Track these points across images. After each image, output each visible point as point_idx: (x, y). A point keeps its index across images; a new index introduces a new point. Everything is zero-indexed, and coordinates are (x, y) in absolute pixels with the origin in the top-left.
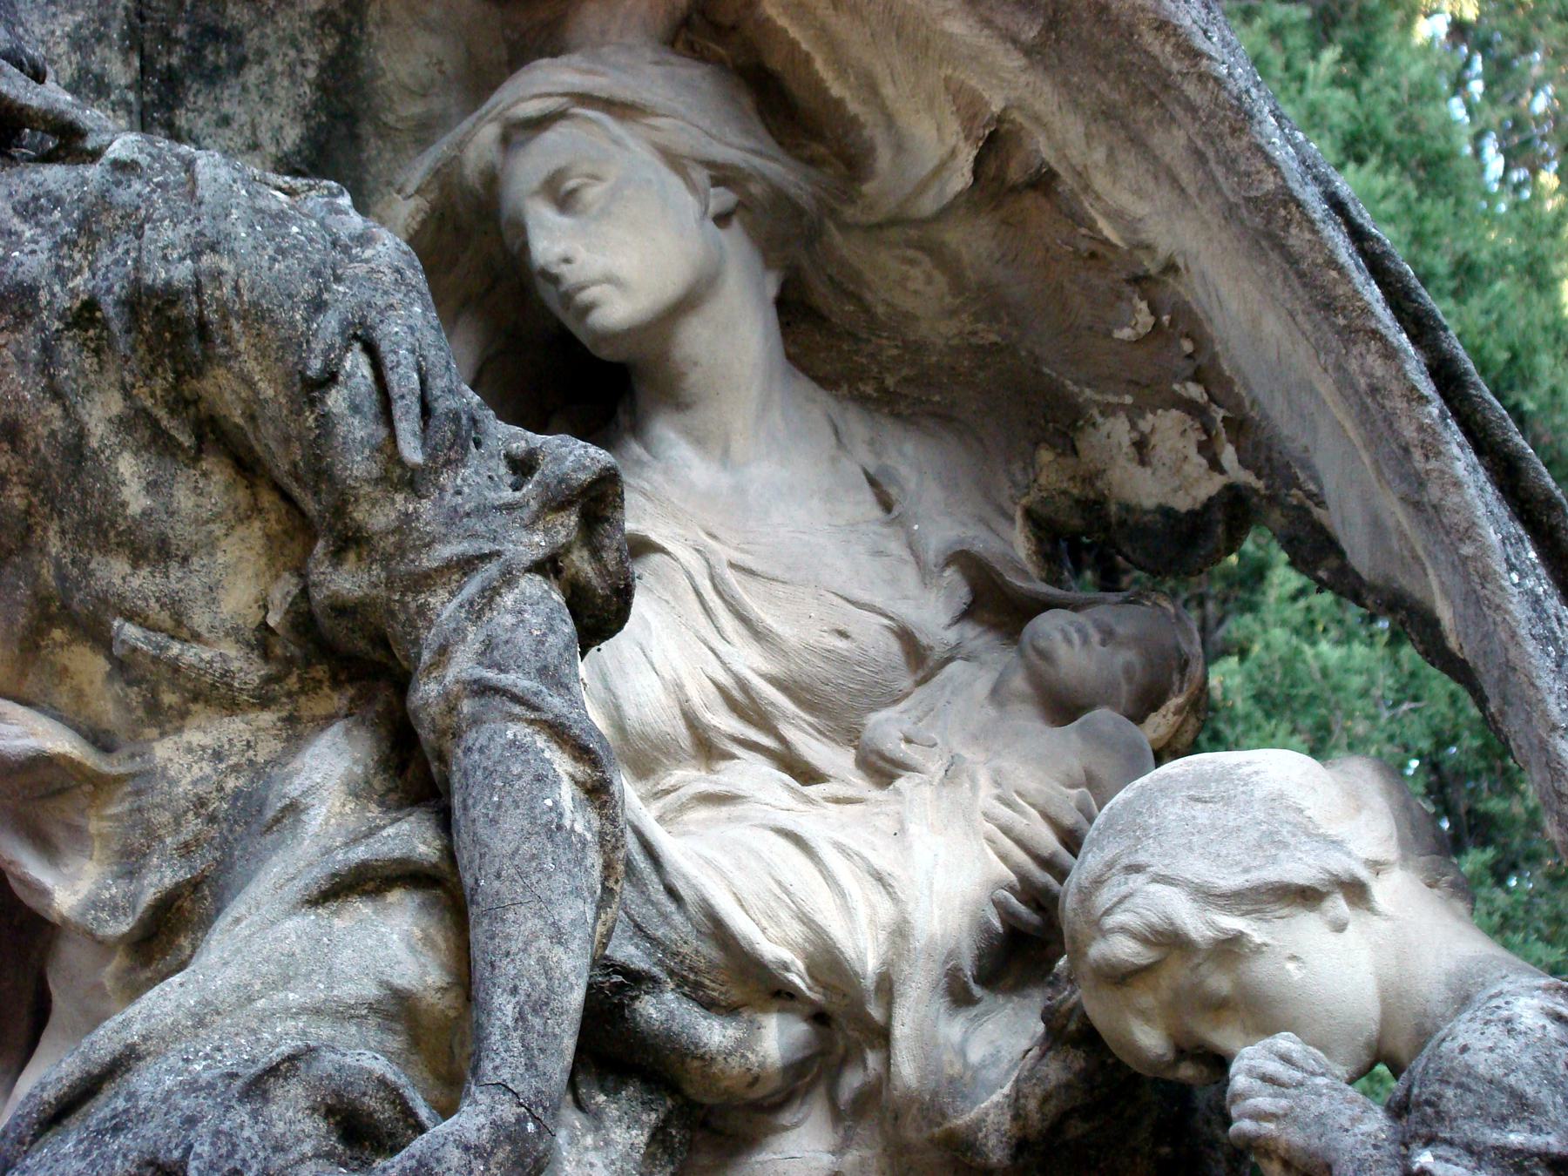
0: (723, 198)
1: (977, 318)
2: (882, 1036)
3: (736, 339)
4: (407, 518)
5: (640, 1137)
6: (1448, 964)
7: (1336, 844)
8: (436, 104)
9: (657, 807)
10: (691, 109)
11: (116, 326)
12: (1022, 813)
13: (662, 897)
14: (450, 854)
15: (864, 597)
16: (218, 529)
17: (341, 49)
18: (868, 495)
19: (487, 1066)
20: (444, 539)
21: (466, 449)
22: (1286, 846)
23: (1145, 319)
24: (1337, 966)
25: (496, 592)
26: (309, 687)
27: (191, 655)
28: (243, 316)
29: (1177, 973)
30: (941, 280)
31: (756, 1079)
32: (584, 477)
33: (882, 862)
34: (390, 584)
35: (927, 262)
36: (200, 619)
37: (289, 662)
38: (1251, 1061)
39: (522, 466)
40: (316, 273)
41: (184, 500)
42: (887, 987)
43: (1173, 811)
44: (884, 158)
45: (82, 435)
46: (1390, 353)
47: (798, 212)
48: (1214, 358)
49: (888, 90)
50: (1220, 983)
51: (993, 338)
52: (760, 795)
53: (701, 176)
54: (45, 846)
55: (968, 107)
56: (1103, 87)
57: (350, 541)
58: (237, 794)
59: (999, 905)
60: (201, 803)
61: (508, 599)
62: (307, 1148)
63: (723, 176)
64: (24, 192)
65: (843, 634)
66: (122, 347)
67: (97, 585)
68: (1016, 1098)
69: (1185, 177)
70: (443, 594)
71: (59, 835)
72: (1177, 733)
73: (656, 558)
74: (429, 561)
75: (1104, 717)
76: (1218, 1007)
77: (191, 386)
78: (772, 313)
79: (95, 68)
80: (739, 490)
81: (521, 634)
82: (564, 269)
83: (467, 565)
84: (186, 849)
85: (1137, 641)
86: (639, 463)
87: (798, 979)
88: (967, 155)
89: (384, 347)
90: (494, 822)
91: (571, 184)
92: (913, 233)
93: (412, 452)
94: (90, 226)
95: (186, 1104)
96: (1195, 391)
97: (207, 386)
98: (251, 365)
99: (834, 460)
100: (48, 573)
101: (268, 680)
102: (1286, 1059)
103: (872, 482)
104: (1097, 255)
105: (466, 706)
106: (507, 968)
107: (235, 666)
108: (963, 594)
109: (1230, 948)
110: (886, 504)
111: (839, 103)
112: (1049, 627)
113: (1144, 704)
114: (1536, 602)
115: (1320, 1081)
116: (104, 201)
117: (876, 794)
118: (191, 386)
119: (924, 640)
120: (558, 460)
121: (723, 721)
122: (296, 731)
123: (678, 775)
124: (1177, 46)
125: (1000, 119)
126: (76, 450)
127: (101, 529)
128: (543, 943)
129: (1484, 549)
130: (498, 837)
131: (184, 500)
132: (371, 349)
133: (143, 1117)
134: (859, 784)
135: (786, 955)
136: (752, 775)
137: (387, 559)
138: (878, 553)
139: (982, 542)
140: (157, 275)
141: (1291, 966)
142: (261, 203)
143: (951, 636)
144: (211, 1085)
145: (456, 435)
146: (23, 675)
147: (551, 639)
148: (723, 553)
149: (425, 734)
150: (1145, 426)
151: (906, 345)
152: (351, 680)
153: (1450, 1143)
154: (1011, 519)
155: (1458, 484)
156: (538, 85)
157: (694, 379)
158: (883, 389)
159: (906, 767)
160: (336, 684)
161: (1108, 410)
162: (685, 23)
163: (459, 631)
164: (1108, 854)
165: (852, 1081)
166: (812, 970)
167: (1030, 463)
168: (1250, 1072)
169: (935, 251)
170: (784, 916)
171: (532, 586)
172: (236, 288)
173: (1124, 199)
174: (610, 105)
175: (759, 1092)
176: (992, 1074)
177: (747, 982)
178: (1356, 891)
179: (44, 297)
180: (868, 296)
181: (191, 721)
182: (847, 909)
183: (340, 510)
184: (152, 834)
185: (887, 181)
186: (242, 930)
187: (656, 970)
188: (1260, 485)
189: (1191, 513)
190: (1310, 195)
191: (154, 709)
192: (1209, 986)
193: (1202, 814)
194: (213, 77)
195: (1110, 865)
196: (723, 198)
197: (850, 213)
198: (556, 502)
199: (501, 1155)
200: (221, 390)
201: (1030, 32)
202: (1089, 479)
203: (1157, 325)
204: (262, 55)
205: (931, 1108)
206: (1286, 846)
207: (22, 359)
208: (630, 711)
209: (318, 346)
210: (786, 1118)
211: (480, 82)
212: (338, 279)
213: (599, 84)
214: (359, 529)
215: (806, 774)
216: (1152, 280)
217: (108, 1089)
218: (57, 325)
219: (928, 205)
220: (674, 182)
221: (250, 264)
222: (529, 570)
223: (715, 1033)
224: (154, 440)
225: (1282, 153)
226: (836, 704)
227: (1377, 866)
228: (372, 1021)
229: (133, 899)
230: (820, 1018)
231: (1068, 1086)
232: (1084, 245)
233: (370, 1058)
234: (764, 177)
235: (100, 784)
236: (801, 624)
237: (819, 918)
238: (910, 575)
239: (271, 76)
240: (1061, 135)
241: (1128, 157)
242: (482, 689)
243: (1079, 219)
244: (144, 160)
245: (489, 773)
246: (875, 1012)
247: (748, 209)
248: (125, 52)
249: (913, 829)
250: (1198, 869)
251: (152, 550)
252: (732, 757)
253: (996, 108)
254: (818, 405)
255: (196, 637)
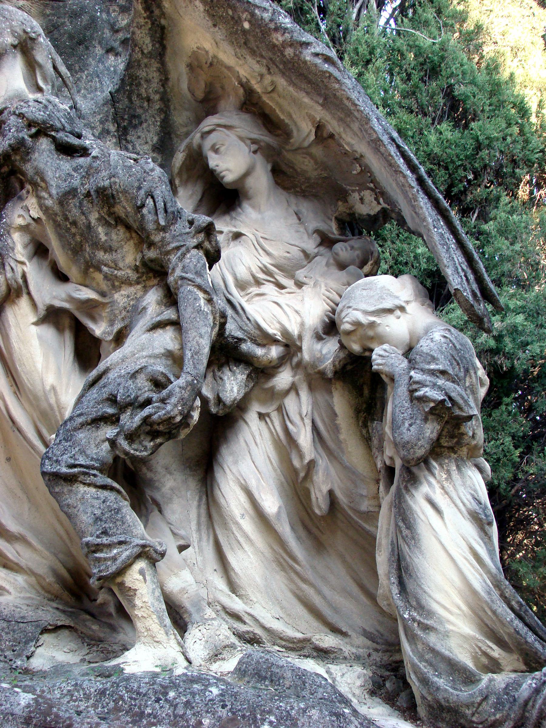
0: (254, 147)
1: (322, 170)
2: (300, 349)
3: (261, 181)
4: (163, 238)
5: (244, 377)
6: (424, 325)
7: (397, 297)
8: (190, 128)
9: (246, 298)
10: (245, 126)
11: (94, 197)
12: (332, 293)
13: (246, 320)
14: (179, 317)
15: (293, 243)
16: (123, 243)
17: (165, 117)
18: (295, 217)
19: (185, 368)
20: (172, 243)
21: (177, 220)
22: (384, 299)
23: (359, 169)
24: (397, 327)
25: (185, 254)
26: (149, 279)
27: (119, 273)
28: (122, 192)
29: (360, 332)
30: (312, 162)
31: (271, 362)
32: (204, 225)
33: (297, 308)
34: (161, 254)
35: (308, 158)
36: (121, 265)
37: (143, 273)
38: (378, 351)
39: (191, 223)
40: (139, 180)
41: (114, 237)
42: (300, 337)
43: (358, 293)
44: (295, 133)
45: (90, 223)
46: (405, 176)
47: (274, 149)
48: (375, 177)
49: (294, 116)
50: (371, 333)
51: (326, 175)
52: (270, 293)
53: (249, 142)
54: (94, 319)
55: (312, 119)
56: (339, 113)
57: (151, 245)
58: (133, 305)
59: (328, 316)
60: (125, 308)
61: (188, 256)
62: (146, 389)
63: (254, 141)
64: (75, 165)
65: (288, 253)
66: (96, 202)
67: (98, 258)
68: (334, 362)
69: (359, 134)
70: (173, 256)
71: (97, 316)
72: (372, 270)
73: (244, 237)
74: (169, 248)
75: (352, 268)
76: (372, 338)
77: (112, 210)
78: (270, 174)
79: (106, 128)
80: (263, 219)
81: (191, 264)
82: (217, 168)
83: (178, 248)
84: (123, 319)
85: (360, 248)
86: (240, 213)
87: (279, 337)
88: (314, 131)
89: (155, 197)
90: (185, 310)
91: (217, 147)
92: (305, 151)
93: (162, 223)
94: (89, 173)
95: (118, 380)
96: (372, 185)
97: (116, 209)
98: (125, 204)
99: (287, 209)
100: (87, 256)
101: (138, 278)
102: (385, 350)
103: (296, 214)
104: (346, 153)
105: (179, 282)
106: (189, 345)
107: (130, 275)
108: (319, 240)
109: (372, 325)
110: (300, 220)
111: (283, 120)
112: (338, 247)
113: (362, 265)
114: (442, 235)
115: (393, 355)
116: (90, 167)
117: (298, 291)
118: (112, 210)
119: (308, 252)
120: (199, 221)
121: (261, 276)
122: (146, 289)
123: (251, 289)
124: (352, 103)
125: (319, 122)
126: (89, 227)
127: (96, 245)
128: (197, 338)
129: (428, 224)
130: (187, 313)
131: (114, 237)
132: (153, 197)
133: (110, 384)
134: (294, 288)
135: (275, 332)
136: (269, 289)
137: (160, 248)
138: (297, 231)
139: (322, 226)
140: (101, 184)
141: (387, 328)
142: (126, 164)
143: (316, 251)
144: (124, 376)
145: (174, 217)
146: (85, 279)
147: (198, 265)
148: (259, 234)
149: (172, 290)
150: (362, 194)
151: (306, 179)
152: (159, 276)
153: (418, 369)
154: (331, 220)
155: (421, 208)
156: (210, 122)
157: (251, 192)
158: (301, 189)
159: (305, 284)
160: (155, 277)
161: (353, 191)
162: (245, 103)
163: (177, 265)
164: (344, 304)
165: (295, 360)
166: (282, 334)
167: (336, 205)
168: (376, 354)
169: (310, 155)
170: (275, 322)
171: (194, 252)
172: (120, 186)
173: (349, 139)
174: (225, 127)
175: (273, 364)
176: (329, 356)
177: (267, 339)
178: (402, 309)
179: (79, 191)
180: (296, 167)
181: (122, 289)
182: (290, 320)
183: (148, 237)
184: (115, 316)
185: (296, 139)
186: (133, 338)
187: (245, 338)
188: (389, 207)
189: (374, 215)
190: (385, 139)
191: (113, 286)
192: (369, 334)
193: (365, 293)
194: (135, 127)
195: (344, 307)
196: (254, 147)
197: (287, 147)
198: (199, 232)
199: (188, 389)
200: (119, 210)
201: (321, 101)
202: (351, 208)
203: (362, 170)
204: (146, 121)
205: (313, 365)
206: (384, 299)
207: (75, 206)
208: (238, 275)
209: (140, 198)
210: (281, 369)
211: (199, 121)
212: (145, 181)
213: (222, 121)
214: (153, 241)
215: (281, 287)
216: (359, 159)
217: (104, 377)
218: (82, 197)
219: (306, 144)
220: (242, 144)
221: (123, 179)
222: (193, 248)
223: (259, 352)
224: (106, 223)
225: (378, 128)
226: (288, 269)
227: (407, 302)
228: (163, 358)
229: (112, 331)
230: (286, 346)
231: (345, 358)
232: (343, 151)
233: (160, 367)
234: (264, 141)
235: (104, 305)
236: (278, 251)
237: (283, 323)
238: (305, 237)
239: (149, 125)
240: (333, 126)
241: (348, 130)
242: (182, 278)
243: (340, 145)
244: (99, 155)
245: (184, 298)
246: (298, 343)
247: (259, 148)
248: (113, 123)
249: (306, 299)
250: (364, 306)
251: (109, 249)
252: (264, 284)
253: (318, 119)
254: (283, 195)
255: (120, 269)
